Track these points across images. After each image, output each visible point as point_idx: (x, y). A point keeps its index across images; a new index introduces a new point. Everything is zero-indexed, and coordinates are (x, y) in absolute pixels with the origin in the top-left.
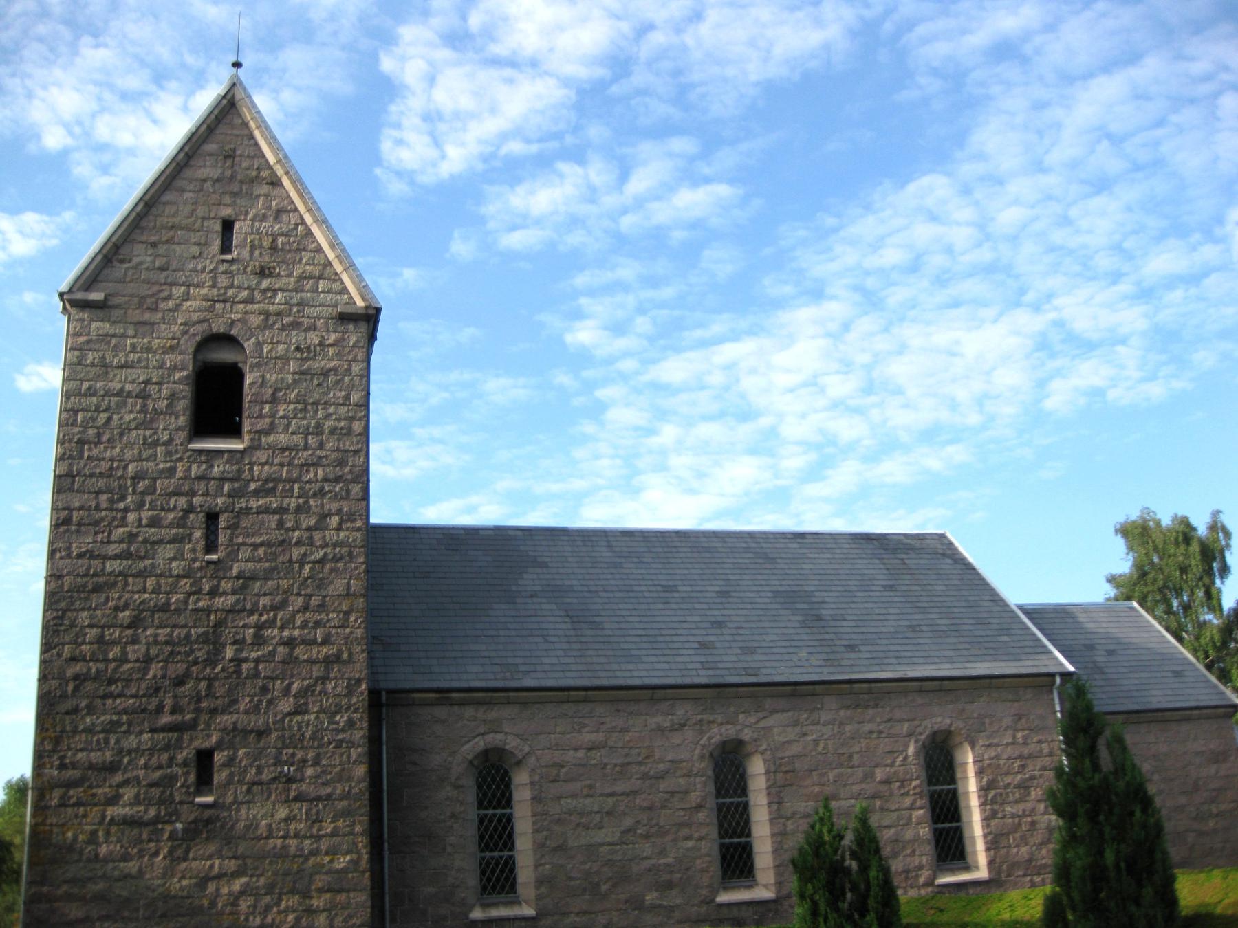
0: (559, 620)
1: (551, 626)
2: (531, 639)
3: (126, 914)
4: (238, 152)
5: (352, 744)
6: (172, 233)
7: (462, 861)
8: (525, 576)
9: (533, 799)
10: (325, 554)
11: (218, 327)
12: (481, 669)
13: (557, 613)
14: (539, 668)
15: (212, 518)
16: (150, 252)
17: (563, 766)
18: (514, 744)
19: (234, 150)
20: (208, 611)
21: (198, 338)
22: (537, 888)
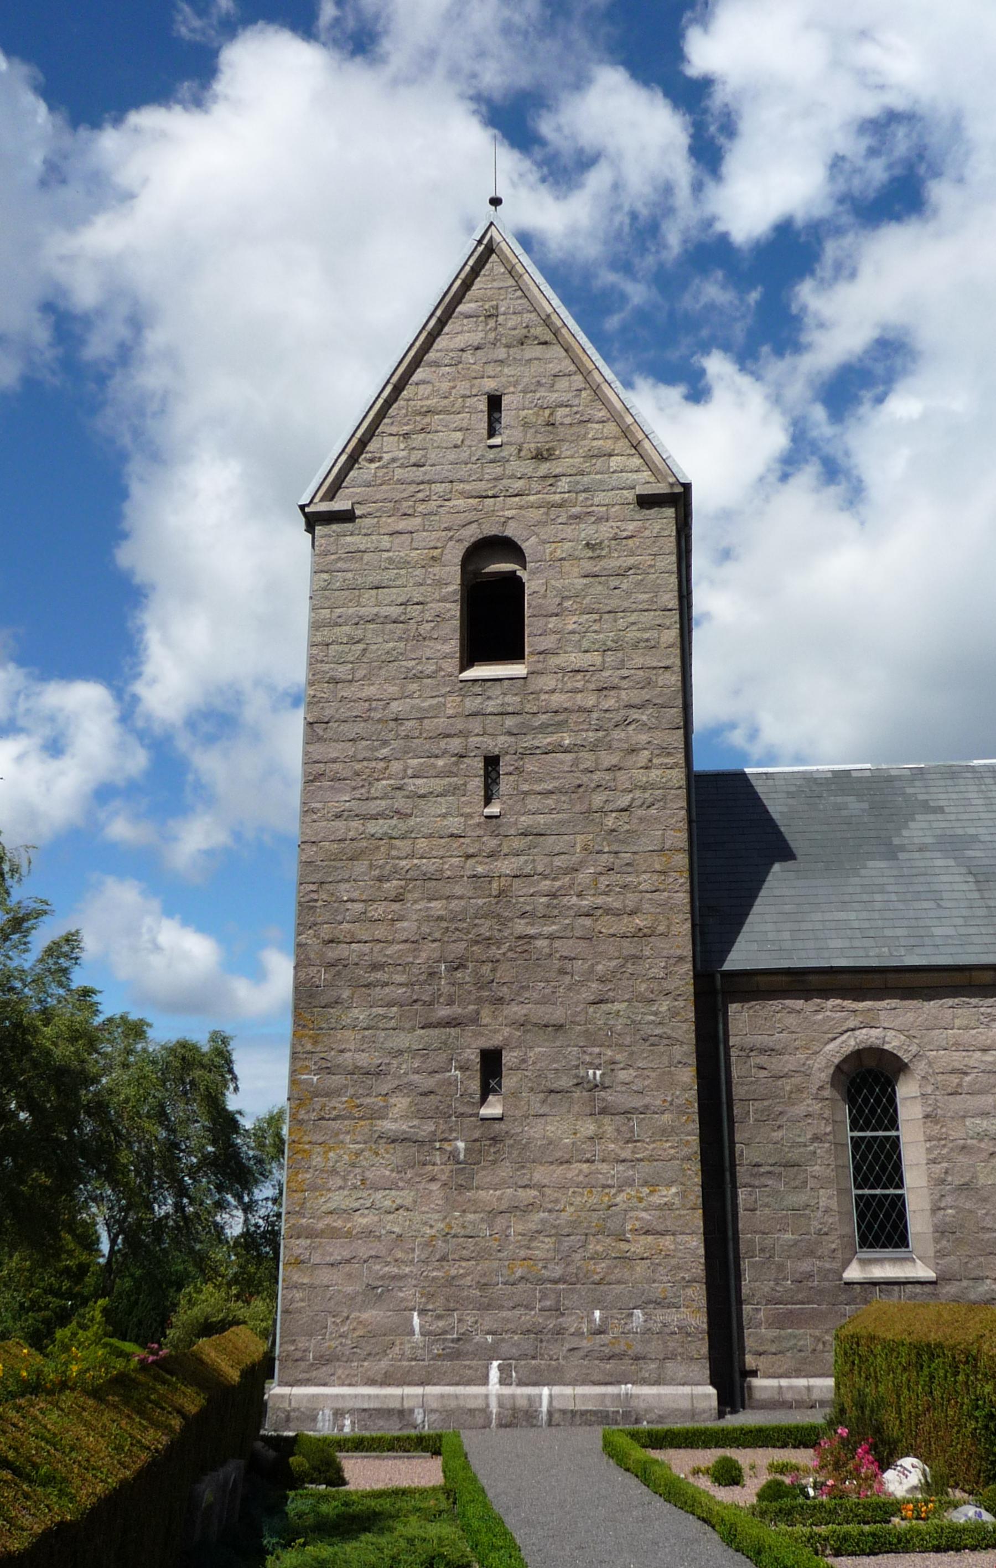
0: (957, 878)
1: (948, 887)
2: (917, 905)
3: (400, 1255)
4: (502, 309)
5: (672, 1041)
6: (427, 420)
7: (829, 1198)
8: (912, 825)
9: (927, 1117)
10: (633, 799)
11: (491, 529)
12: (847, 943)
13: (955, 870)
14: (927, 941)
15: (492, 762)
16: (402, 446)
17: (966, 1074)
18: (895, 1043)
19: (497, 307)
20: (489, 877)
21: (467, 544)
22: (937, 1241)
